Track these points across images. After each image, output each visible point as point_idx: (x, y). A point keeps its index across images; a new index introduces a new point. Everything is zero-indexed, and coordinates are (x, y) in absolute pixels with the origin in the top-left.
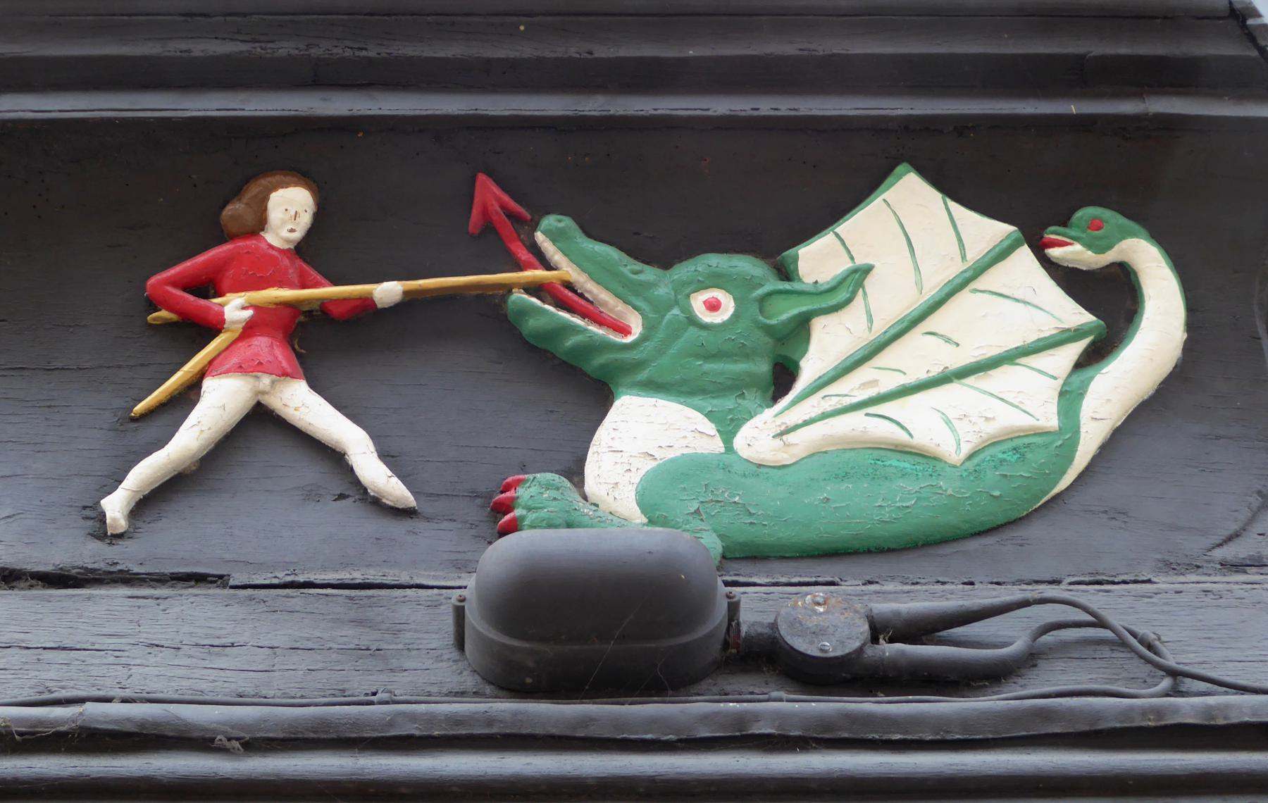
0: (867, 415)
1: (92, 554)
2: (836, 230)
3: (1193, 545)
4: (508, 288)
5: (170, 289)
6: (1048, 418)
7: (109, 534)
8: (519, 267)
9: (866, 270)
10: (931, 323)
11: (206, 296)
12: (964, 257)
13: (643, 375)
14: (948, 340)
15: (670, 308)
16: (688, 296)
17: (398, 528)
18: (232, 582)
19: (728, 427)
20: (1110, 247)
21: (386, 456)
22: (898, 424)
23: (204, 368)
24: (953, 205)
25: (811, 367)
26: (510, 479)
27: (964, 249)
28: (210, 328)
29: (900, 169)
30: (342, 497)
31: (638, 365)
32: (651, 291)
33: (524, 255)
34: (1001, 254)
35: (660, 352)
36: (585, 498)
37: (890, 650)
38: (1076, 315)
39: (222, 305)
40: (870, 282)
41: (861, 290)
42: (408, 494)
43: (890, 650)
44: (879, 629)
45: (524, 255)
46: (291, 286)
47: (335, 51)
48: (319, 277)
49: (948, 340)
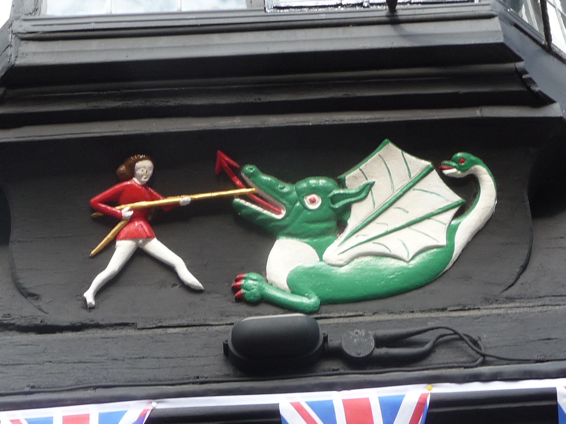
0: (373, 243)
1: (84, 317)
2: (361, 167)
3: (497, 290)
4: (232, 197)
5: (100, 204)
6: (443, 241)
7: (88, 307)
8: (237, 187)
9: (372, 184)
10: (397, 204)
11: (114, 205)
12: (410, 176)
13: (286, 231)
14: (405, 211)
15: (296, 203)
16: (303, 197)
17: (196, 298)
18: (139, 327)
19: (320, 250)
20: (467, 170)
21: (190, 268)
22: (385, 246)
23: (116, 235)
24: (407, 156)
25: (353, 222)
26: (238, 277)
27: (410, 173)
28: (116, 219)
29: (386, 140)
30: (174, 285)
31: (285, 227)
32: (289, 196)
33: (238, 182)
34: (426, 174)
35: (293, 221)
36: (267, 281)
37: (383, 351)
38: (456, 198)
39: (121, 210)
40: (373, 189)
41: (370, 192)
42: (200, 285)
43: (383, 351)
44: (380, 342)
45: (238, 182)
46: (147, 200)
47: (157, 103)
48: (158, 196)
49: (405, 211)
